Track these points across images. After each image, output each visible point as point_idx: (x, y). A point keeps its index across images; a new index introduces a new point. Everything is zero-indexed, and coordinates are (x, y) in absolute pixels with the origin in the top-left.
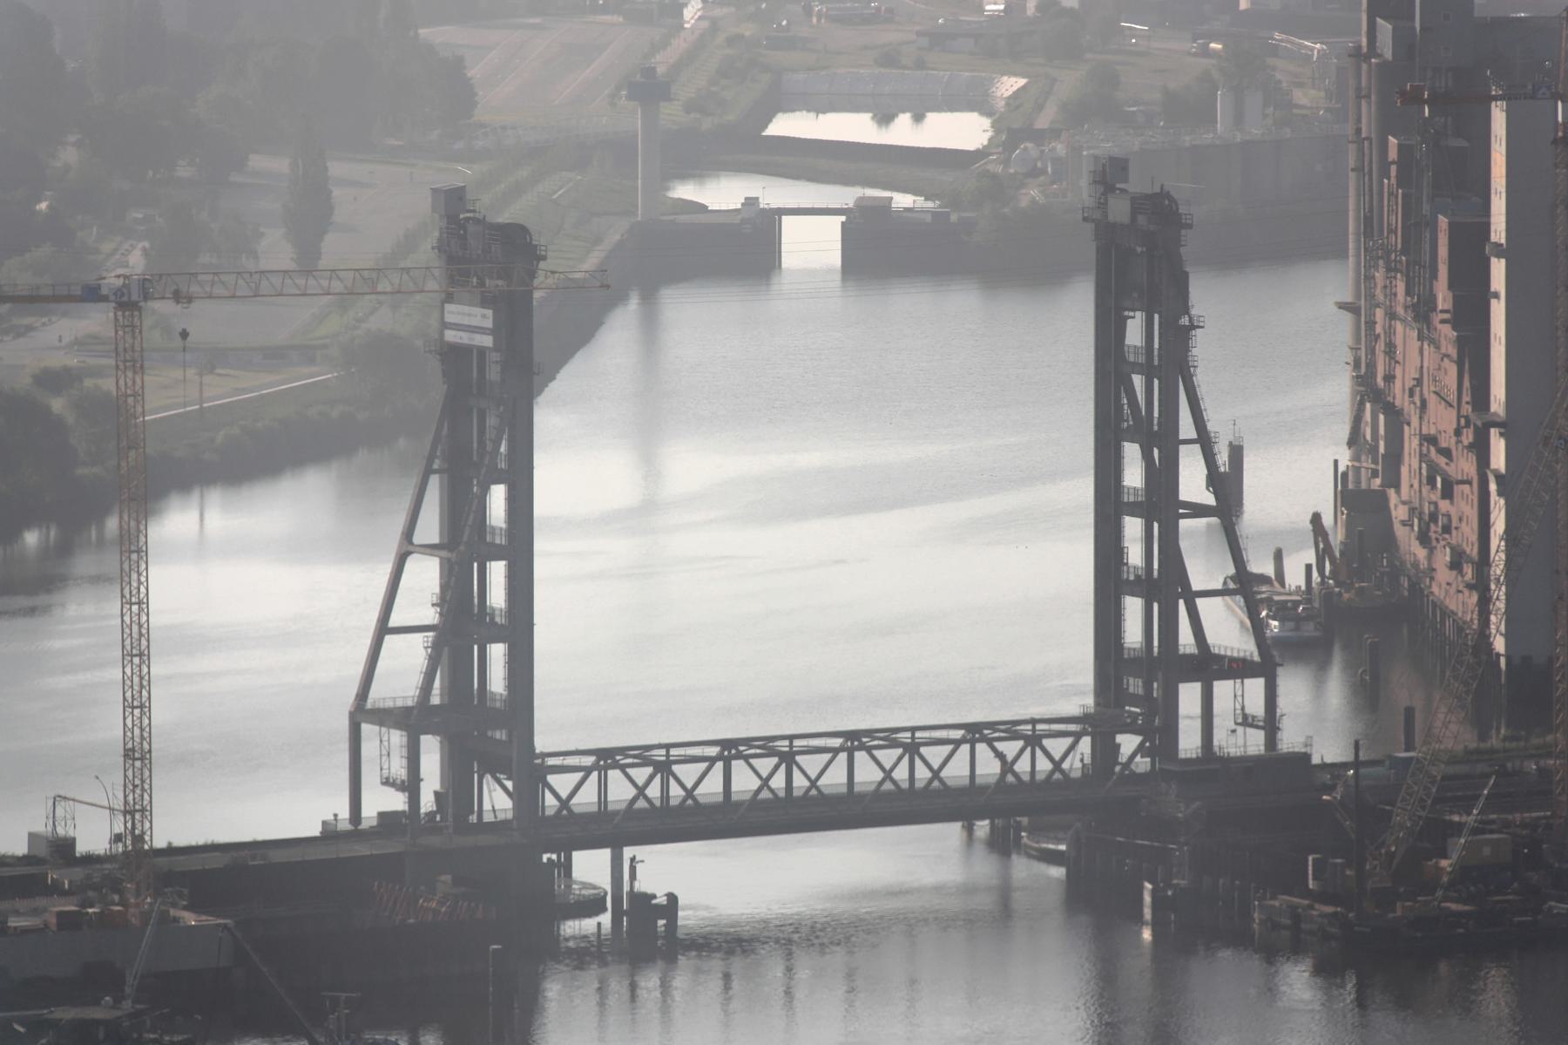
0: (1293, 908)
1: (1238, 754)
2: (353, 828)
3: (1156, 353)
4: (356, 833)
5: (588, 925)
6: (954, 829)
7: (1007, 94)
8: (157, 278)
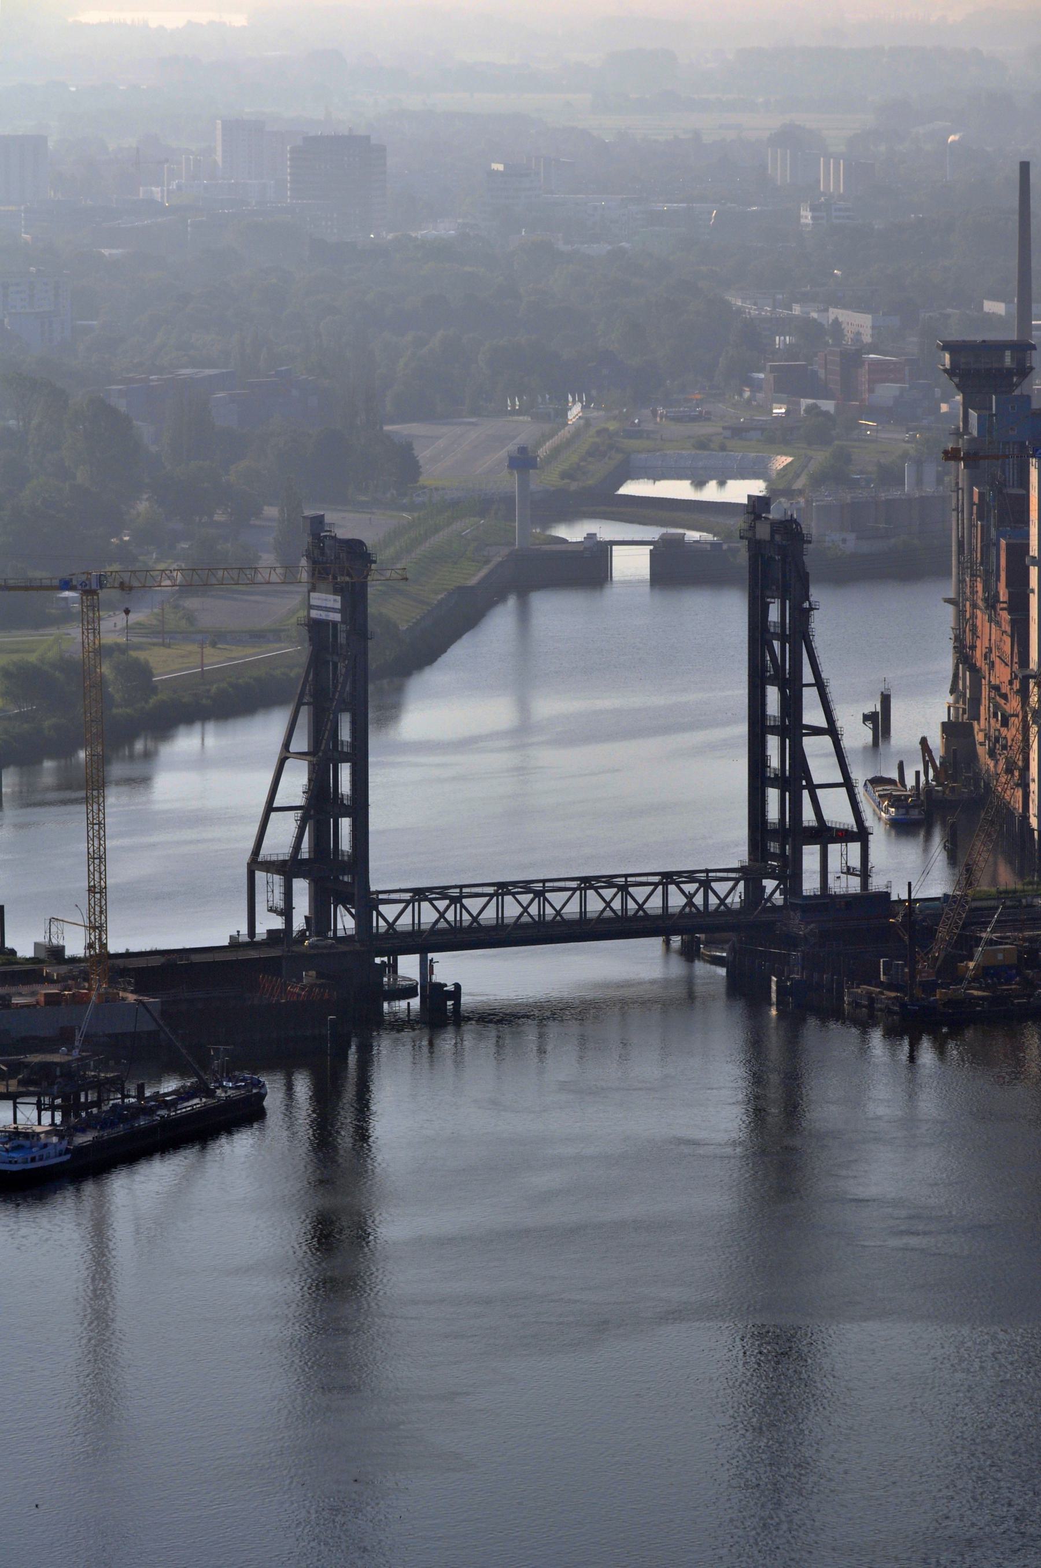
0: (869, 993)
1: (842, 893)
2: (250, 940)
3: (787, 626)
4: (252, 944)
5: (402, 1005)
6: (657, 942)
7: (779, 468)
8: (109, 574)
